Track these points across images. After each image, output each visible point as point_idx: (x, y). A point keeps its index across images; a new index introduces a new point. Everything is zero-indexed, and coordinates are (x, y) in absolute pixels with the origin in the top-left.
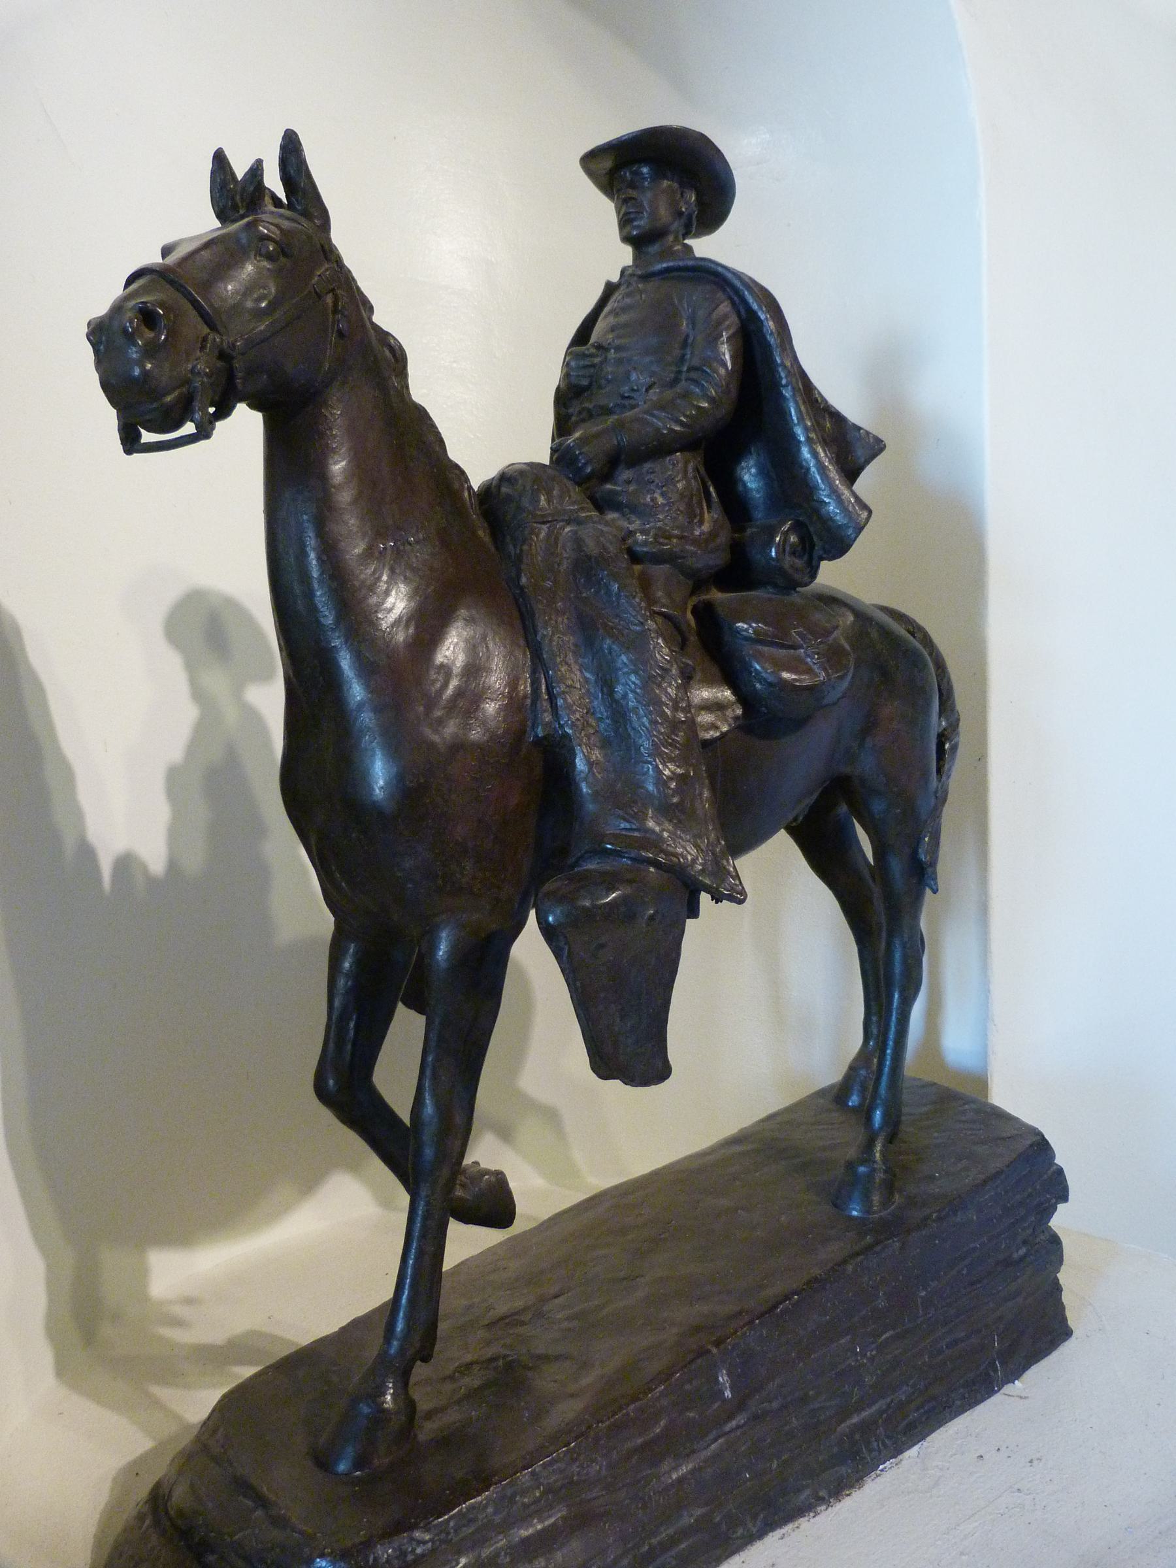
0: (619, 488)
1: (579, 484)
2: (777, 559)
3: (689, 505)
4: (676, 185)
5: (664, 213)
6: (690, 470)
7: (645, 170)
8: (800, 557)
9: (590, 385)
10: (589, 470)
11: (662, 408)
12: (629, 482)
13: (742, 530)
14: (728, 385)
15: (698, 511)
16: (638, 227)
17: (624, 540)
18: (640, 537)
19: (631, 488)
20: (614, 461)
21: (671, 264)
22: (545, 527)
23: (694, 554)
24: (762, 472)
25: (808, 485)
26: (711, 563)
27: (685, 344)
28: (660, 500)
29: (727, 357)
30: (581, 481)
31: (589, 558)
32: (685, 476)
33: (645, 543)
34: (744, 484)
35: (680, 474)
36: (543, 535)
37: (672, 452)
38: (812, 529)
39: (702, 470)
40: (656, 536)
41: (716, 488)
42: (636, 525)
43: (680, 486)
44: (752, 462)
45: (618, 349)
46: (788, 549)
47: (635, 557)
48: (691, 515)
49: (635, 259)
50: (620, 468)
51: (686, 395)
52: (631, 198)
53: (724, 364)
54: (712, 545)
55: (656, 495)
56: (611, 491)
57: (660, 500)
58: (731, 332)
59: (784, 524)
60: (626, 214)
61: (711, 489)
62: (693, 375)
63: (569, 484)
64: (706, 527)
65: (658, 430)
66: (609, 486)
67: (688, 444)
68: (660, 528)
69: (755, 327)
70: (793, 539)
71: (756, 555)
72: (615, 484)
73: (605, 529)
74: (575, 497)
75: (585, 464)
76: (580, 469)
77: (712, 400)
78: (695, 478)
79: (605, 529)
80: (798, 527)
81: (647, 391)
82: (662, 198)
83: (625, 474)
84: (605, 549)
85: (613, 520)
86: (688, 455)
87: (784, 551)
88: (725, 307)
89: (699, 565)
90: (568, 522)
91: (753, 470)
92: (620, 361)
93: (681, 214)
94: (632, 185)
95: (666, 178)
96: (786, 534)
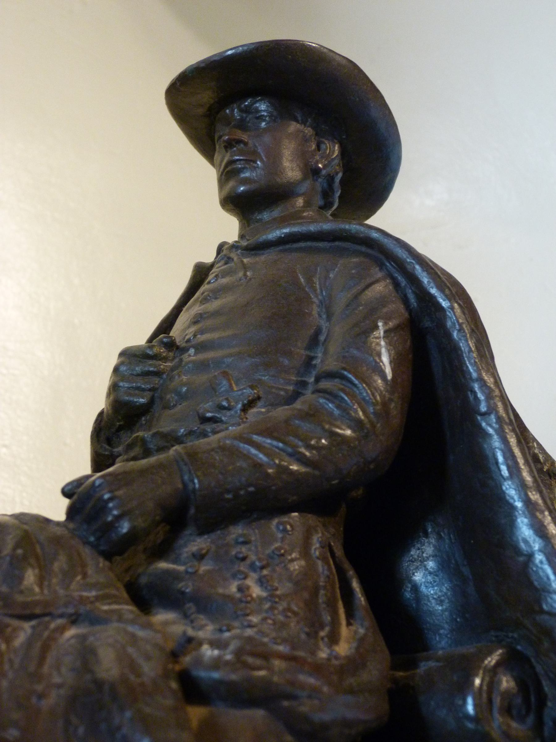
0: (182, 568)
1: (108, 556)
2: (475, 719)
3: (311, 604)
4: (309, 131)
5: (291, 170)
6: (316, 549)
7: (263, 106)
8: (521, 719)
9: (152, 402)
10: (125, 527)
11: (268, 432)
12: (200, 557)
13: (412, 664)
14: (385, 404)
15: (327, 618)
16: (245, 181)
17: (175, 655)
18: (209, 652)
19: (204, 567)
20: (177, 518)
21: (296, 229)
22: (27, 626)
23: (314, 692)
24: (446, 565)
25: (530, 584)
26: (350, 715)
27: (314, 341)
28: (256, 591)
29: (385, 359)
30: (113, 549)
31: (99, 684)
32: (306, 553)
33: (217, 664)
34: (415, 588)
35: (297, 547)
36: (20, 640)
37: (286, 510)
38: (539, 668)
39: (339, 552)
40: (238, 653)
41: (362, 582)
42: (207, 631)
43: (295, 567)
44: (429, 550)
45: (201, 347)
46: (497, 701)
47: (192, 690)
48: (314, 625)
49: (243, 227)
50: (187, 532)
51: (312, 414)
52: (239, 141)
53: (383, 376)
54: (351, 681)
55: (249, 582)
56: (167, 572)
57: (256, 591)
58: (391, 324)
59: (490, 653)
60: (231, 162)
61: (355, 585)
62: (325, 384)
63: (86, 552)
64: (343, 649)
65: (257, 466)
66: (163, 565)
67: (317, 499)
68: (250, 639)
69: (436, 335)
70: (506, 683)
71: (436, 710)
72: (175, 562)
73: (141, 633)
74: (93, 576)
75: (118, 518)
76: (111, 526)
77: (357, 425)
78: (323, 559)
79: (141, 633)
80: (514, 661)
81: (245, 409)
82: (291, 152)
83: (197, 544)
84: (134, 667)
85: (166, 623)
86: (312, 519)
87: (490, 701)
88: (381, 288)
89: (326, 717)
90: (75, 620)
91: (431, 564)
92: (203, 366)
93: (316, 172)
94: (242, 126)
95: (291, 124)
96: (494, 671)
